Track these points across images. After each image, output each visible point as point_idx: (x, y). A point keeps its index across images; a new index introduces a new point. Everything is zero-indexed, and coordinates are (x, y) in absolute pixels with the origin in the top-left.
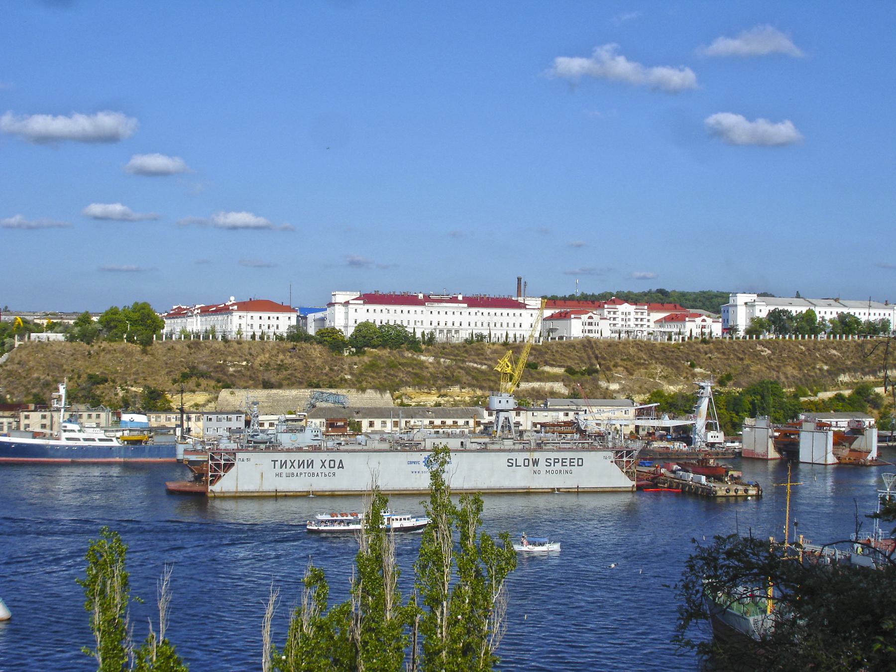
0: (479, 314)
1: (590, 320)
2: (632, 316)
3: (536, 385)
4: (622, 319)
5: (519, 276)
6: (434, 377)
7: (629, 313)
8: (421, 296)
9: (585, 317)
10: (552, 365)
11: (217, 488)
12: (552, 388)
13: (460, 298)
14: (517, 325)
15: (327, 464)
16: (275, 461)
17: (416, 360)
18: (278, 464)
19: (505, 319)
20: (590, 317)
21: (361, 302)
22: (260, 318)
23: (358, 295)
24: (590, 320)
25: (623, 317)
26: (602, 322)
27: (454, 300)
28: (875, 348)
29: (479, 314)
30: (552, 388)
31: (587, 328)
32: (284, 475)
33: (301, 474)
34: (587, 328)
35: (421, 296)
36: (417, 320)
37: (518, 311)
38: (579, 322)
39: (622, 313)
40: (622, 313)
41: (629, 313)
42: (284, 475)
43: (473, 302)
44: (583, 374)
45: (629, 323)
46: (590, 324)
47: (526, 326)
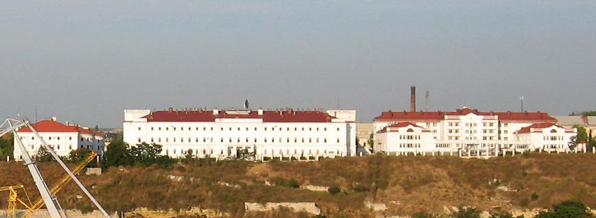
0: (277, 129)
2: (480, 128)
4: (467, 131)
6: (176, 196)
7: (475, 124)
8: (216, 112)
13: (260, 112)
14: (322, 140)
17: (162, 178)
19: (208, 134)
21: (146, 120)
22: (70, 138)
23: (147, 112)
24: (410, 134)
25: (468, 128)
27: (254, 115)
28: (69, 201)
29: (171, 129)
31: (407, 141)
34: (407, 141)
35: (216, 112)
37: (321, 125)
39: (467, 125)
40: (467, 125)
41: (475, 124)
43: (270, 117)
44: (553, 193)
45: (474, 135)
46: (410, 138)
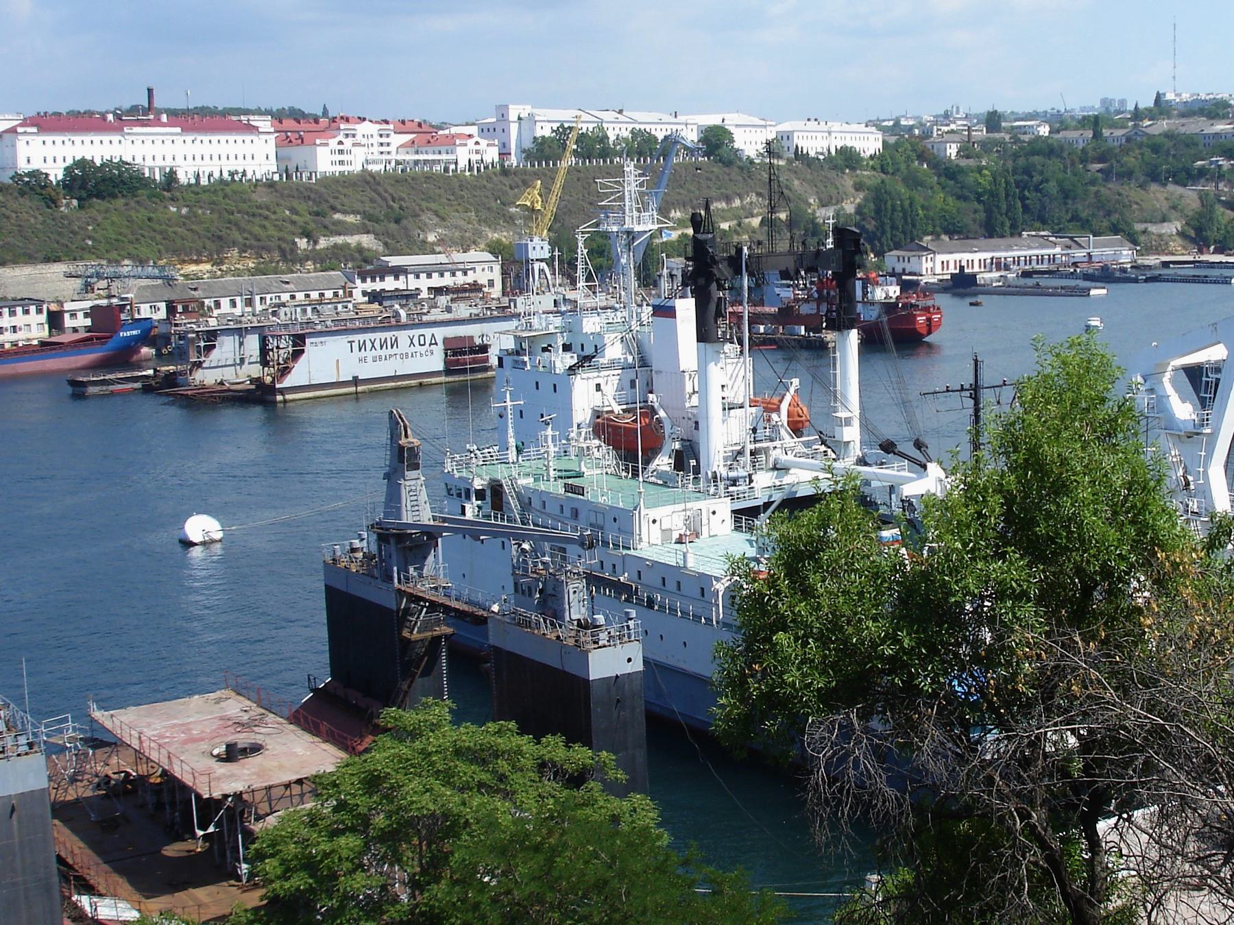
1: (341, 147)
3: (339, 240)
5: (151, 86)
9: (333, 143)
10: (345, 212)
11: (288, 382)
12: (359, 244)
15: (416, 341)
16: (351, 342)
18: (355, 345)
20: (341, 143)
24: (341, 147)
26: (355, 150)
30: (359, 244)
31: (339, 157)
32: (370, 359)
33: (391, 356)
34: (339, 157)
36: (151, 150)
38: (326, 150)
42: (370, 359)
46: (341, 152)
47: (260, 158)
